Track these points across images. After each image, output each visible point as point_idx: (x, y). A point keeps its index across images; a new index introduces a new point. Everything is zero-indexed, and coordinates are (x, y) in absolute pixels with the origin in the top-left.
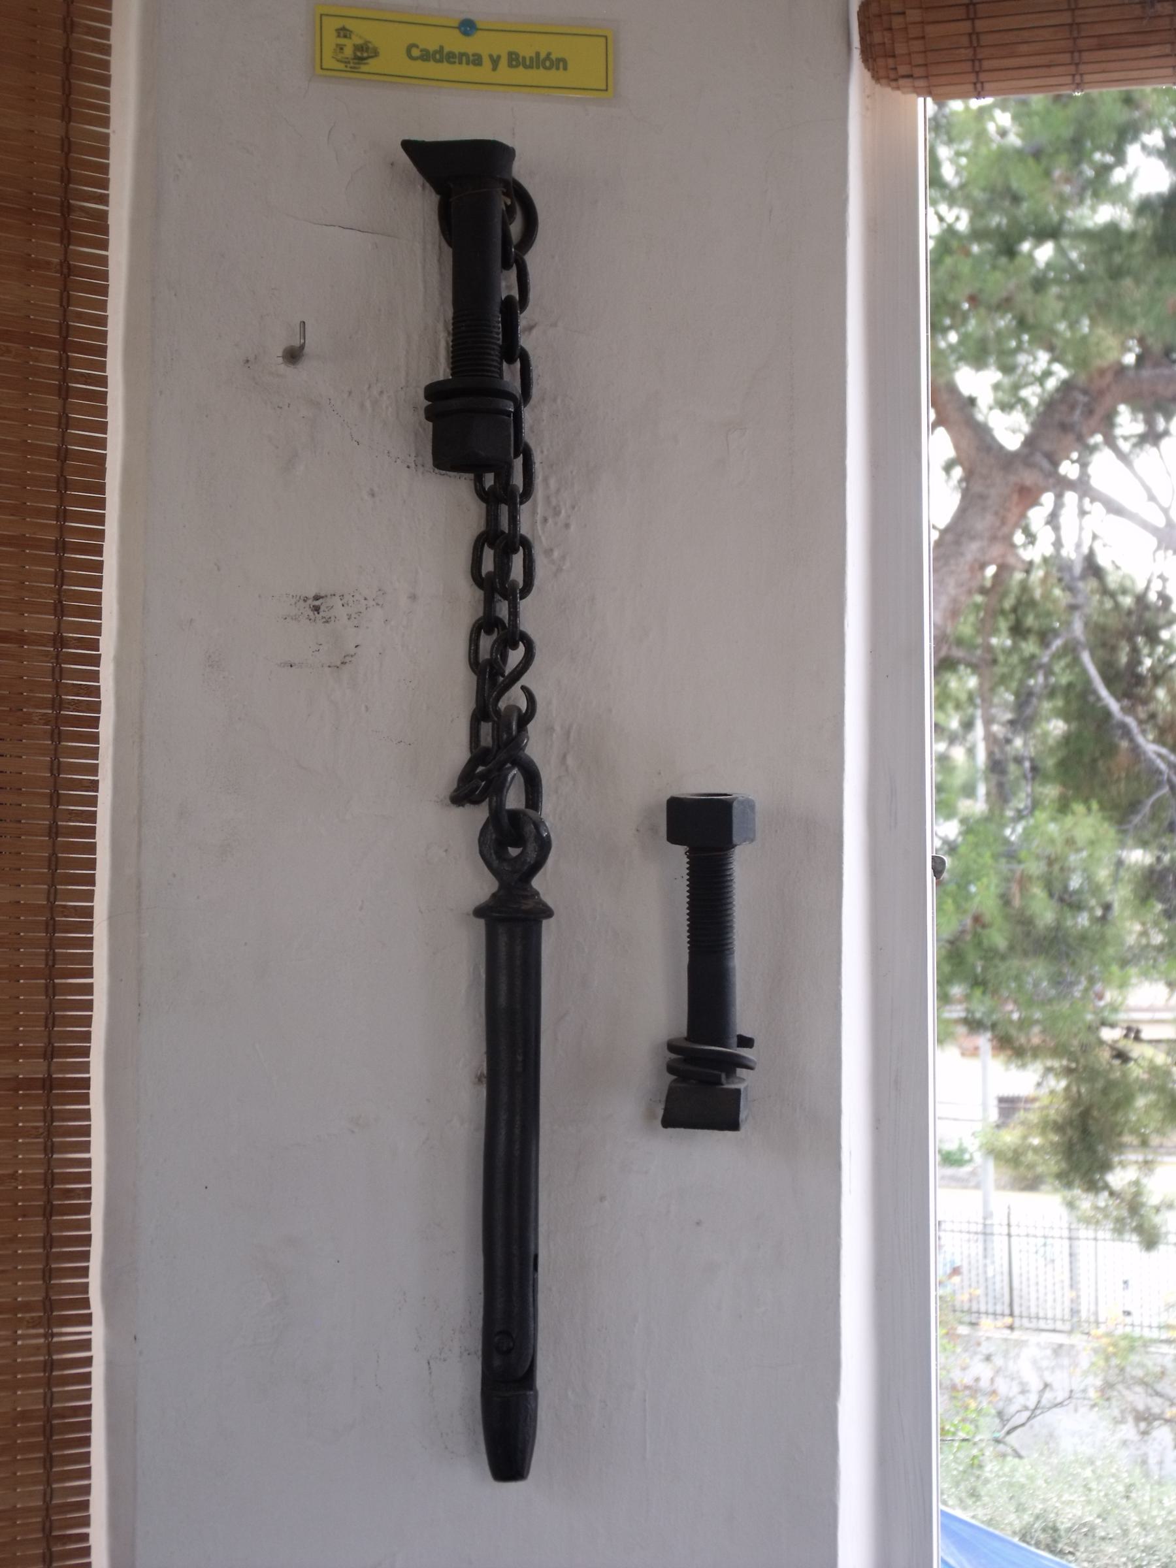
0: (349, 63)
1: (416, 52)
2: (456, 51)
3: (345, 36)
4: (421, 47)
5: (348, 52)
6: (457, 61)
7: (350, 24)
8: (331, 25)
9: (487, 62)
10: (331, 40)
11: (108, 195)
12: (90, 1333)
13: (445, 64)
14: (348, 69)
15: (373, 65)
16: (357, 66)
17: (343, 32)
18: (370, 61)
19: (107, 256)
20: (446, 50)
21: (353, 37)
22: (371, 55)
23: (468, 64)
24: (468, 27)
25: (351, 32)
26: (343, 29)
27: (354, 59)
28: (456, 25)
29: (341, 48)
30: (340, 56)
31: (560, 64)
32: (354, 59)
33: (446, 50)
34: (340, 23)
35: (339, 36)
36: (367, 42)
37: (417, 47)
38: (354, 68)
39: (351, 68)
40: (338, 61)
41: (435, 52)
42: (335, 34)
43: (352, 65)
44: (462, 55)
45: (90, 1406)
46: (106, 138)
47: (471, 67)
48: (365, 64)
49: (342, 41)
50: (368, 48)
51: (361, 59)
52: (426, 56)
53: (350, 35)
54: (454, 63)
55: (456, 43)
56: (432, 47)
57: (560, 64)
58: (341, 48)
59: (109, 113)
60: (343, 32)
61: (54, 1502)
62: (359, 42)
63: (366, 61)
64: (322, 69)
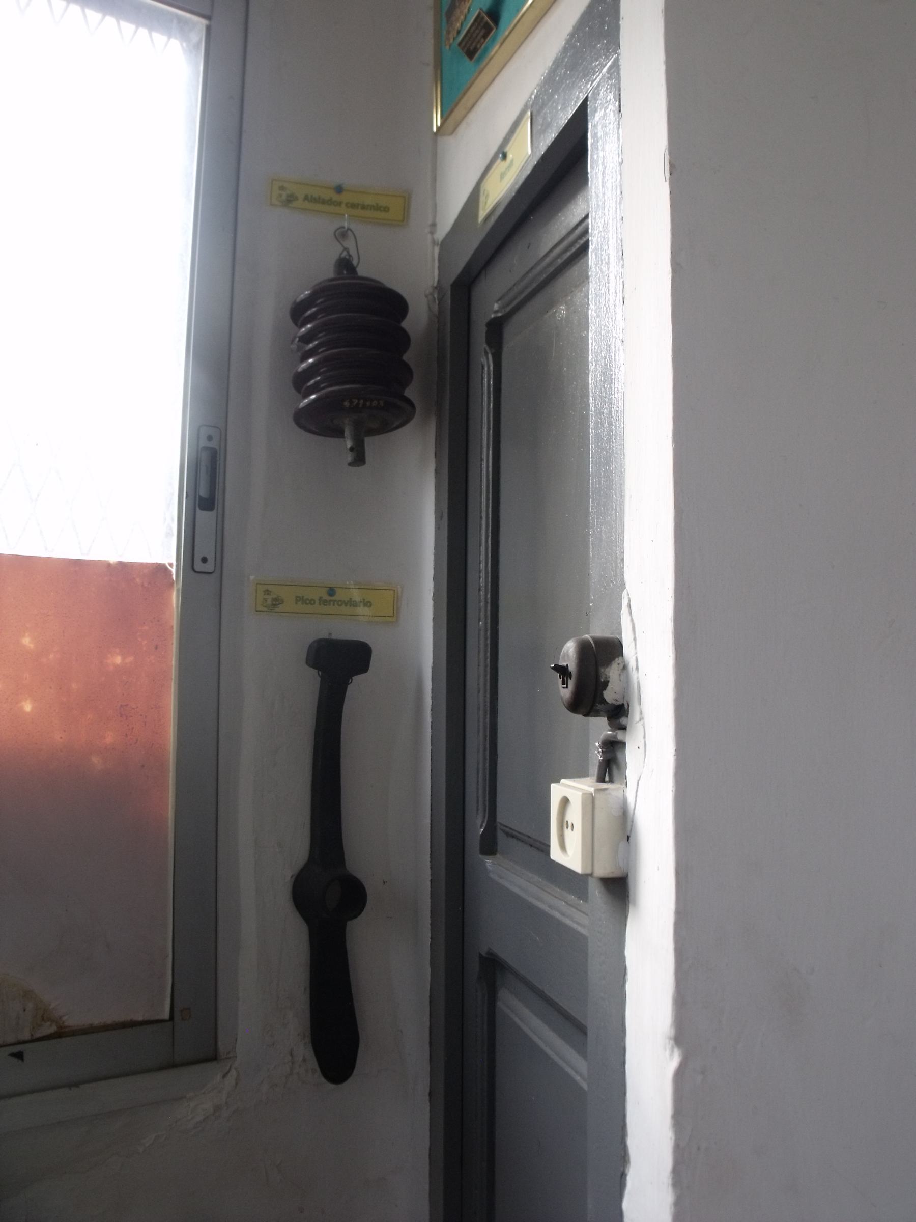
25: (271, 592)
26: (267, 590)
27: (272, 605)
30: (265, 605)
32: (272, 605)
54: (326, 605)
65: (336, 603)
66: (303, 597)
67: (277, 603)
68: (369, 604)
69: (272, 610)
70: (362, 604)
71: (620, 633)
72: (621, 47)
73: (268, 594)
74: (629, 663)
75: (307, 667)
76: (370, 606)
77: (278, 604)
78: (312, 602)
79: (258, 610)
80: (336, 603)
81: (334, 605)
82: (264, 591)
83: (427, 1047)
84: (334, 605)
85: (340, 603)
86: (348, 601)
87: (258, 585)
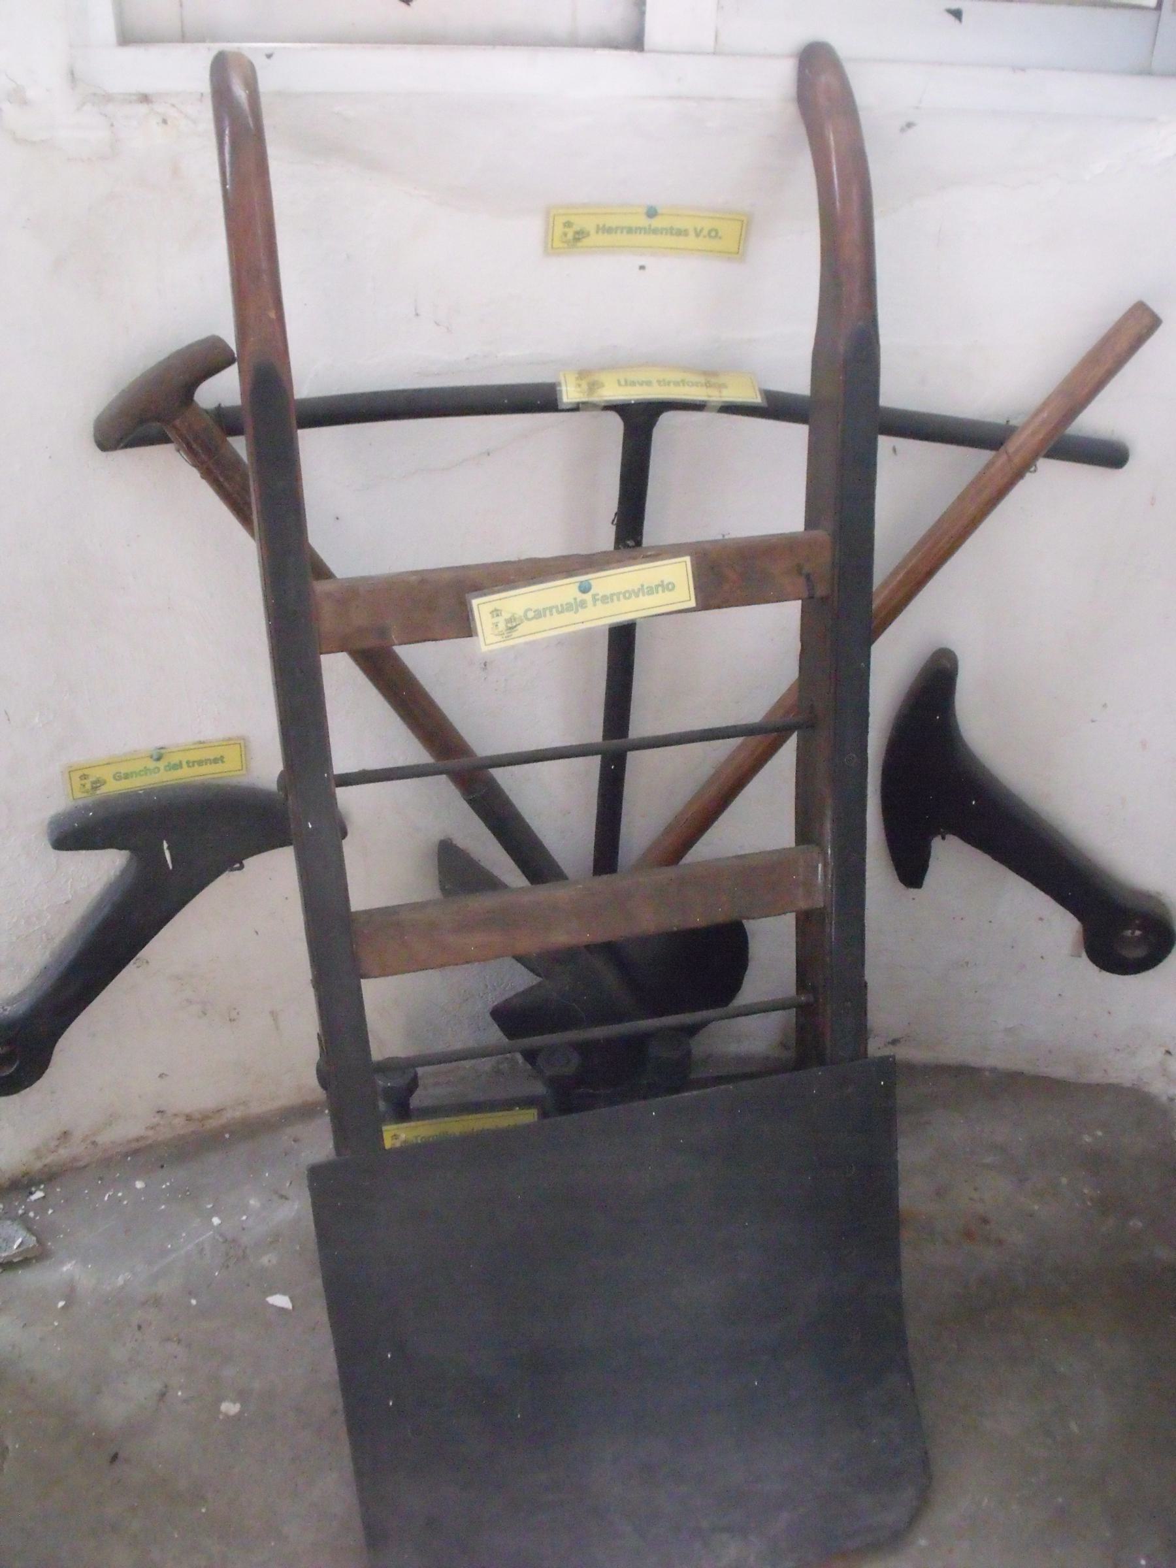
0: (504, 634)
2: (608, 593)
6: (609, 600)
8: (560, 221)
9: (692, 233)
10: (559, 229)
12: (657, 593)
14: (505, 639)
15: (586, 242)
16: (510, 634)
17: (568, 224)
18: (518, 627)
21: (503, 613)
22: (518, 623)
24: (652, 213)
25: (501, 611)
26: (496, 610)
27: (507, 630)
29: (565, 234)
30: (496, 632)
32: (507, 630)
35: (493, 617)
38: (508, 637)
39: (506, 637)
40: (496, 635)
42: (490, 616)
43: (506, 635)
48: (515, 631)
50: (515, 619)
53: (501, 613)
54: (608, 602)
55: (643, 222)
58: (565, 234)
60: (568, 224)
63: (515, 629)
64: (486, 645)
65: (621, 596)
66: (662, 582)
67: (514, 624)
68: (670, 586)
69: (508, 637)
70: (660, 589)
71: (590, 634)
72: (316, 1036)
73: (498, 615)
74: (254, 784)
75: (54, 850)
76: (674, 587)
77: (515, 626)
78: (670, 586)
79: (689, 599)
80: (621, 596)
81: (551, 614)
82: (492, 612)
83: (798, 662)
84: (551, 614)
85: (627, 595)
86: (639, 590)
87: (684, 564)
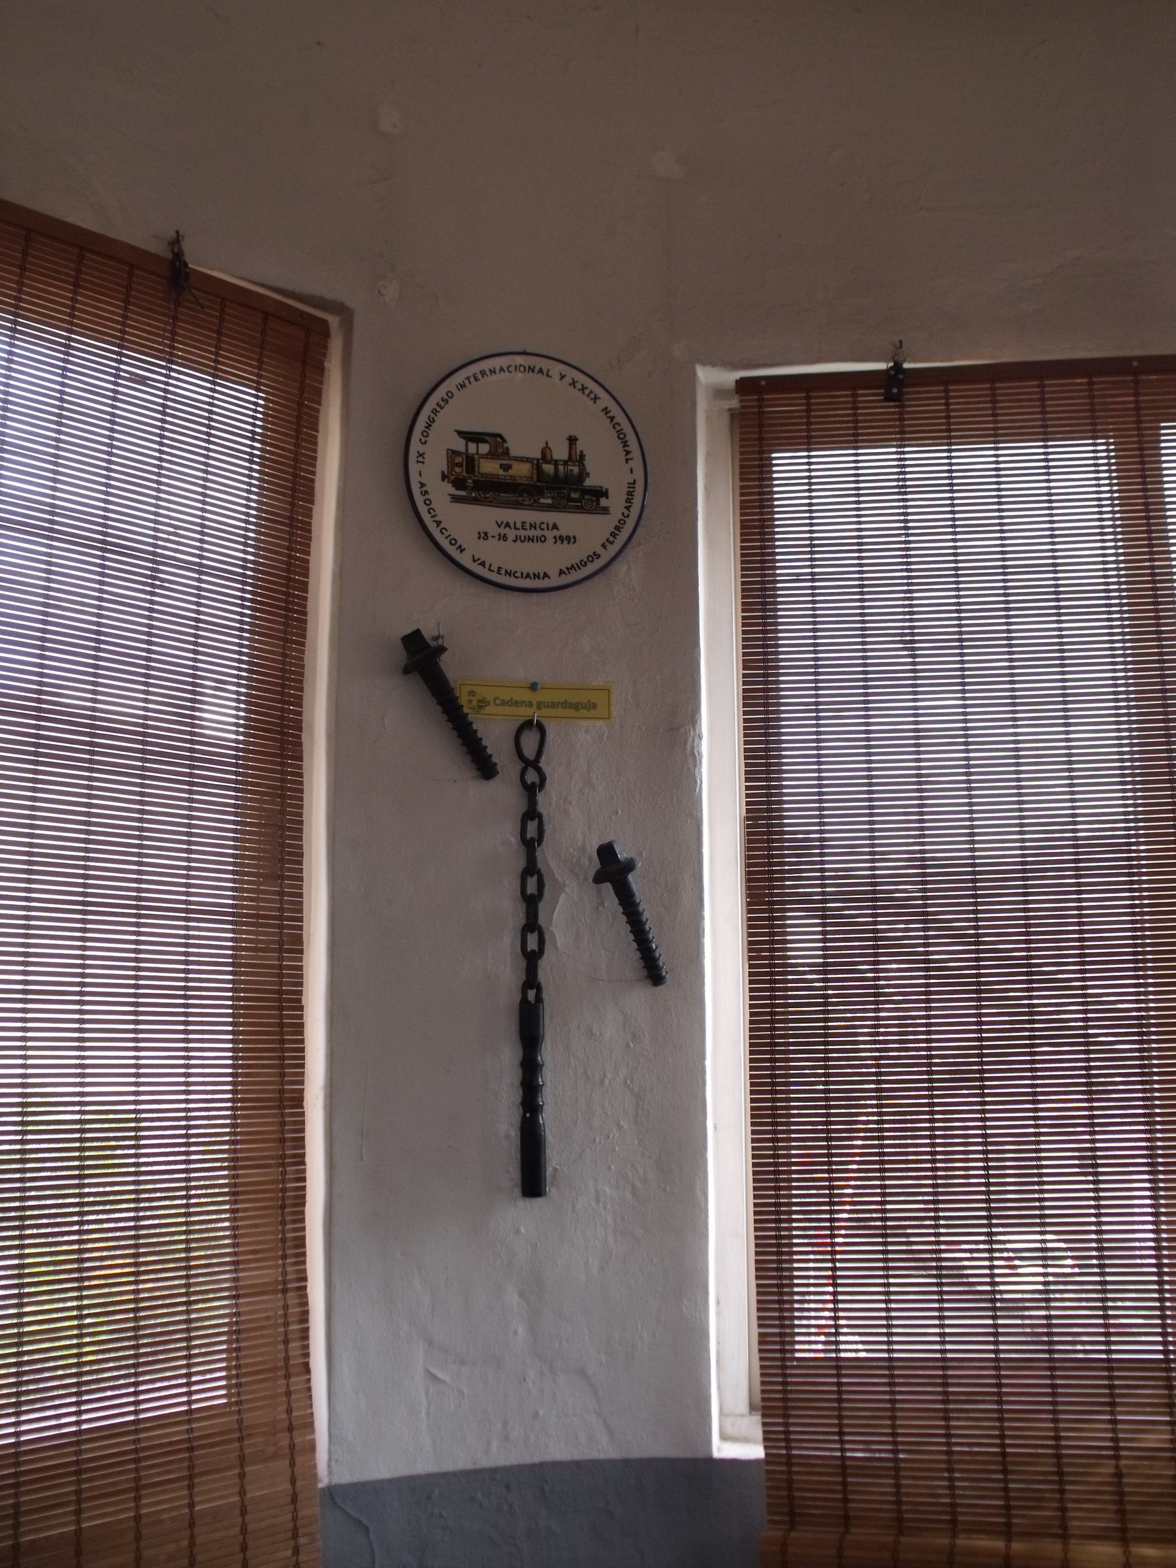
1: (498, 702)
3: (473, 695)
4: (501, 698)
5: (475, 703)
7: (474, 688)
11: (302, 966)
13: (514, 707)
19: (307, 597)
20: (514, 699)
23: (525, 706)
24: (533, 687)
26: (472, 691)
28: (528, 686)
31: (595, 706)
33: (514, 699)
34: (469, 688)
36: (484, 698)
37: (499, 698)
41: (509, 701)
44: (548, 707)
45: (303, 1089)
46: (316, 437)
47: (527, 708)
49: (472, 698)
51: (481, 707)
52: (504, 703)
55: (526, 695)
56: (507, 698)
57: (595, 706)
58: (471, 701)
59: (311, 519)
61: (288, 1278)
62: (480, 698)
